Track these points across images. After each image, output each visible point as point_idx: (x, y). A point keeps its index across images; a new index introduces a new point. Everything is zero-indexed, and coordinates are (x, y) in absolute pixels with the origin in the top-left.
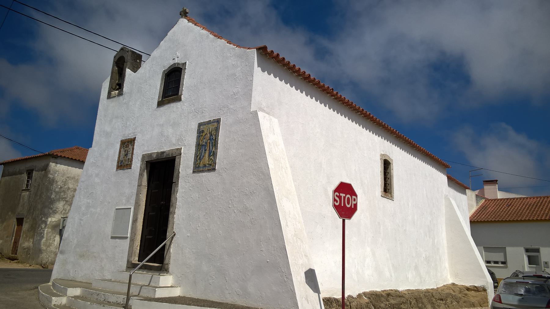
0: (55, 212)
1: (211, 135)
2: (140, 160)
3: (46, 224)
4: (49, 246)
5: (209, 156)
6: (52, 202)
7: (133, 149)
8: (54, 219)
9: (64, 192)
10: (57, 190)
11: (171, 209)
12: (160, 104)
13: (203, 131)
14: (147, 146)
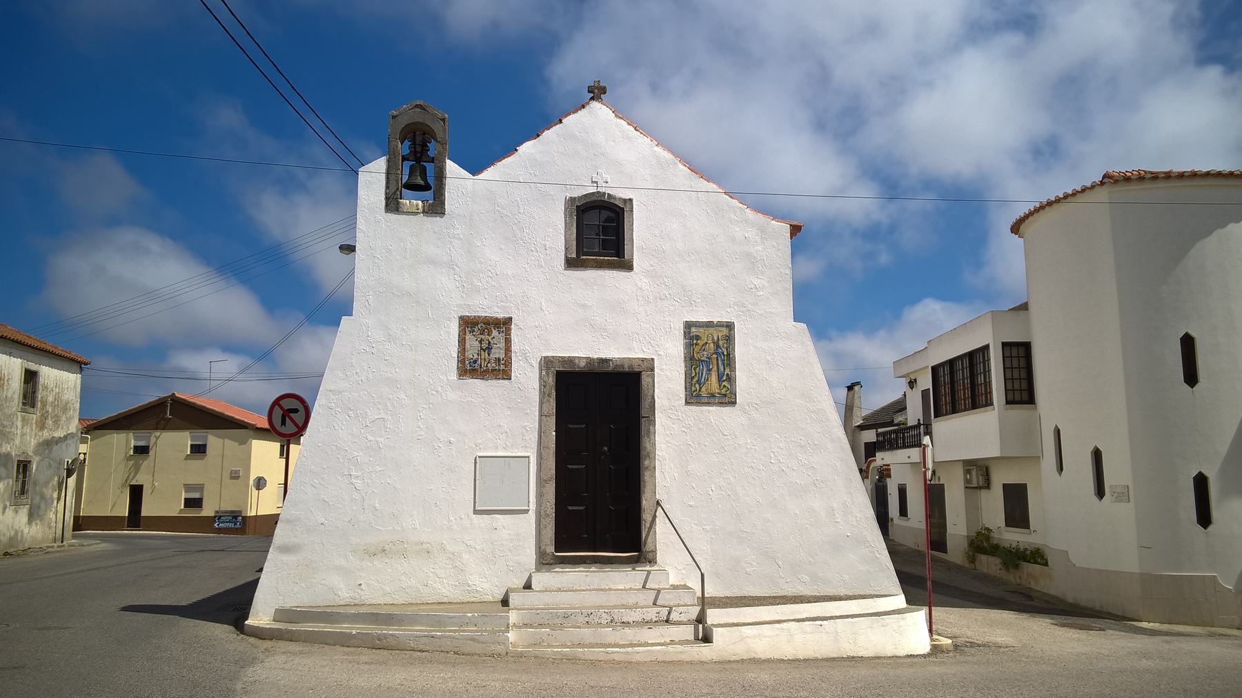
1: (718, 346)
2: (536, 366)
5: (720, 380)
7: (508, 341)
13: (698, 338)
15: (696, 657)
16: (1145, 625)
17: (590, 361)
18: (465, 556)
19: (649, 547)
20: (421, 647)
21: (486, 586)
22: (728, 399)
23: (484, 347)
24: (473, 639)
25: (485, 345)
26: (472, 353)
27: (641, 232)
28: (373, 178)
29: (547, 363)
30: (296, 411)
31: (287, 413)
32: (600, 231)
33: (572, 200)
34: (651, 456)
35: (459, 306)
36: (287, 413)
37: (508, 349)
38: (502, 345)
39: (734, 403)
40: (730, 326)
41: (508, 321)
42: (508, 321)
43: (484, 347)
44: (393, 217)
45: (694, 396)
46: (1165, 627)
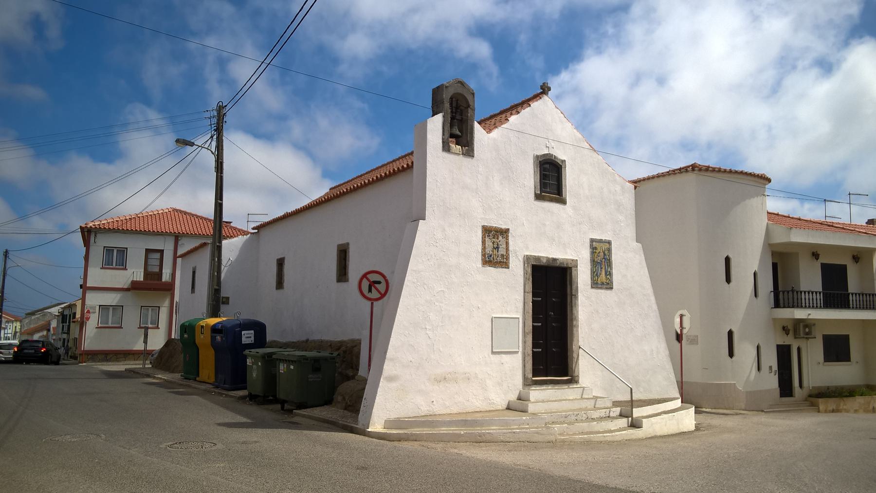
1: (605, 254)
2: (522, 260)
5: (606, 275)
7: (507, 244)
11: (575, 323)
13: (596, 248)
15: (634, 437)
16: (704, 409)
17: (548, 259)
18: (488, 381)
19: (576, 374)
20: (508, 440)
21: (498, 400)
22: (608, 286)
23: (495, 246)
24: (537, 433)
25: (495, 246)
26: (489, 250)
27: (571, 179)
28: (435, 125)
29: (527, 259)
30: (379, 283)
31: (372, 284)
32: (550, 178)
33: (537, 157)
34: (576, 319)
35: (482, 219)
36: (372, 284)
37: (507, 249)
38: (504, 246)
39: (612, 288)
40: (609, 243)
41: (507, 231)
42: (507, 231)
43: (495, 246)
44: (446, 155)
45: (595, 284)
46: (714, 411)
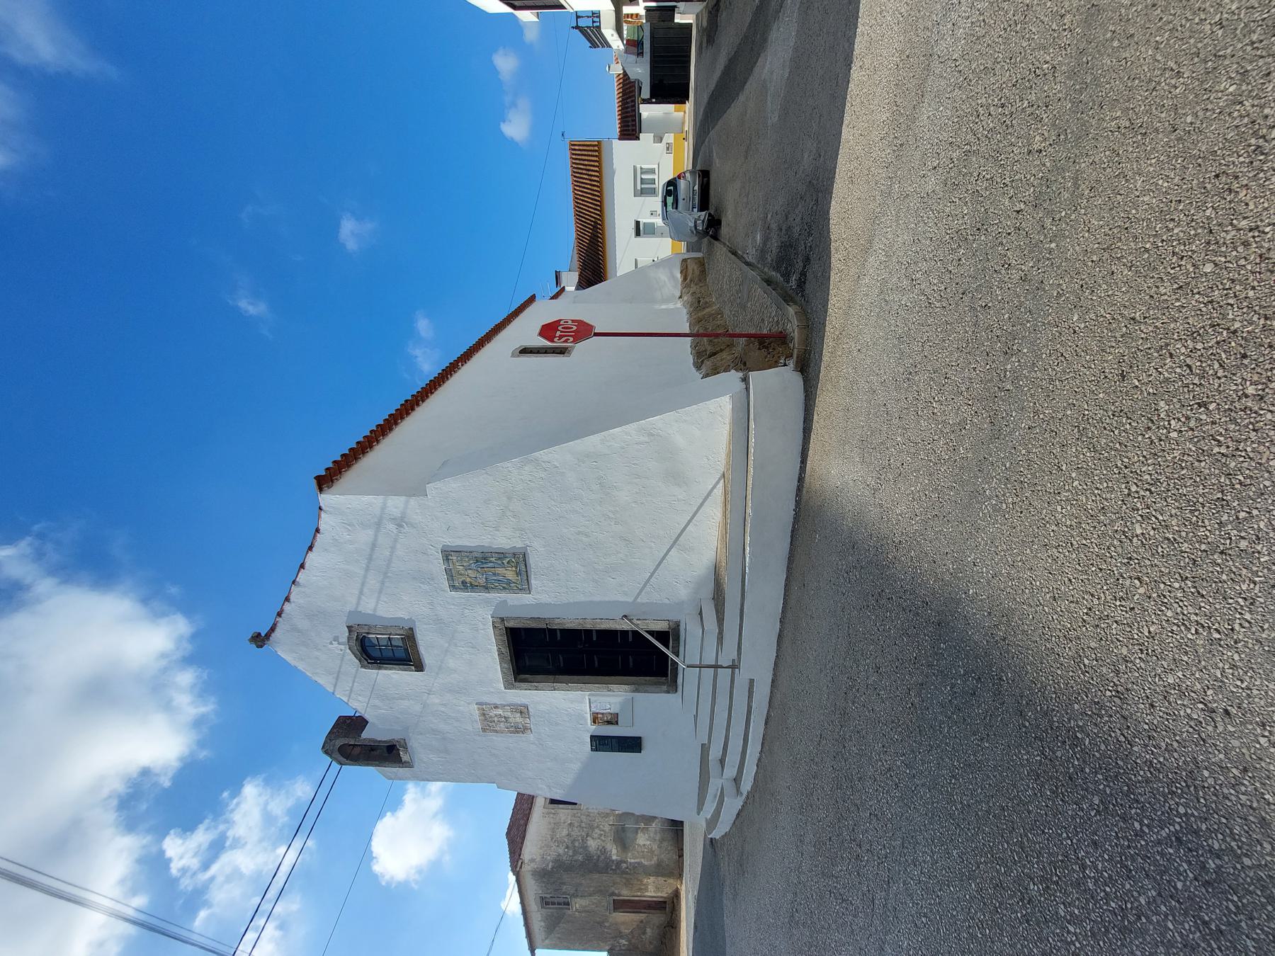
0: (604, 851)
3: (622, 862)
4: (652, 852)
6: (589, 857)
8: (614, 851)
9: (573, 842)
10: (571, 853)
12: (420, 667)
13: (464, 583)
14: (489, 660)
29: (508, 686)
